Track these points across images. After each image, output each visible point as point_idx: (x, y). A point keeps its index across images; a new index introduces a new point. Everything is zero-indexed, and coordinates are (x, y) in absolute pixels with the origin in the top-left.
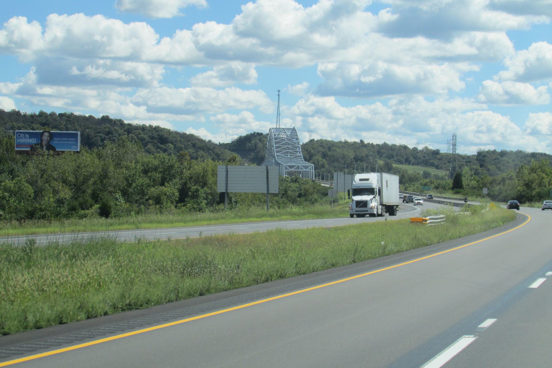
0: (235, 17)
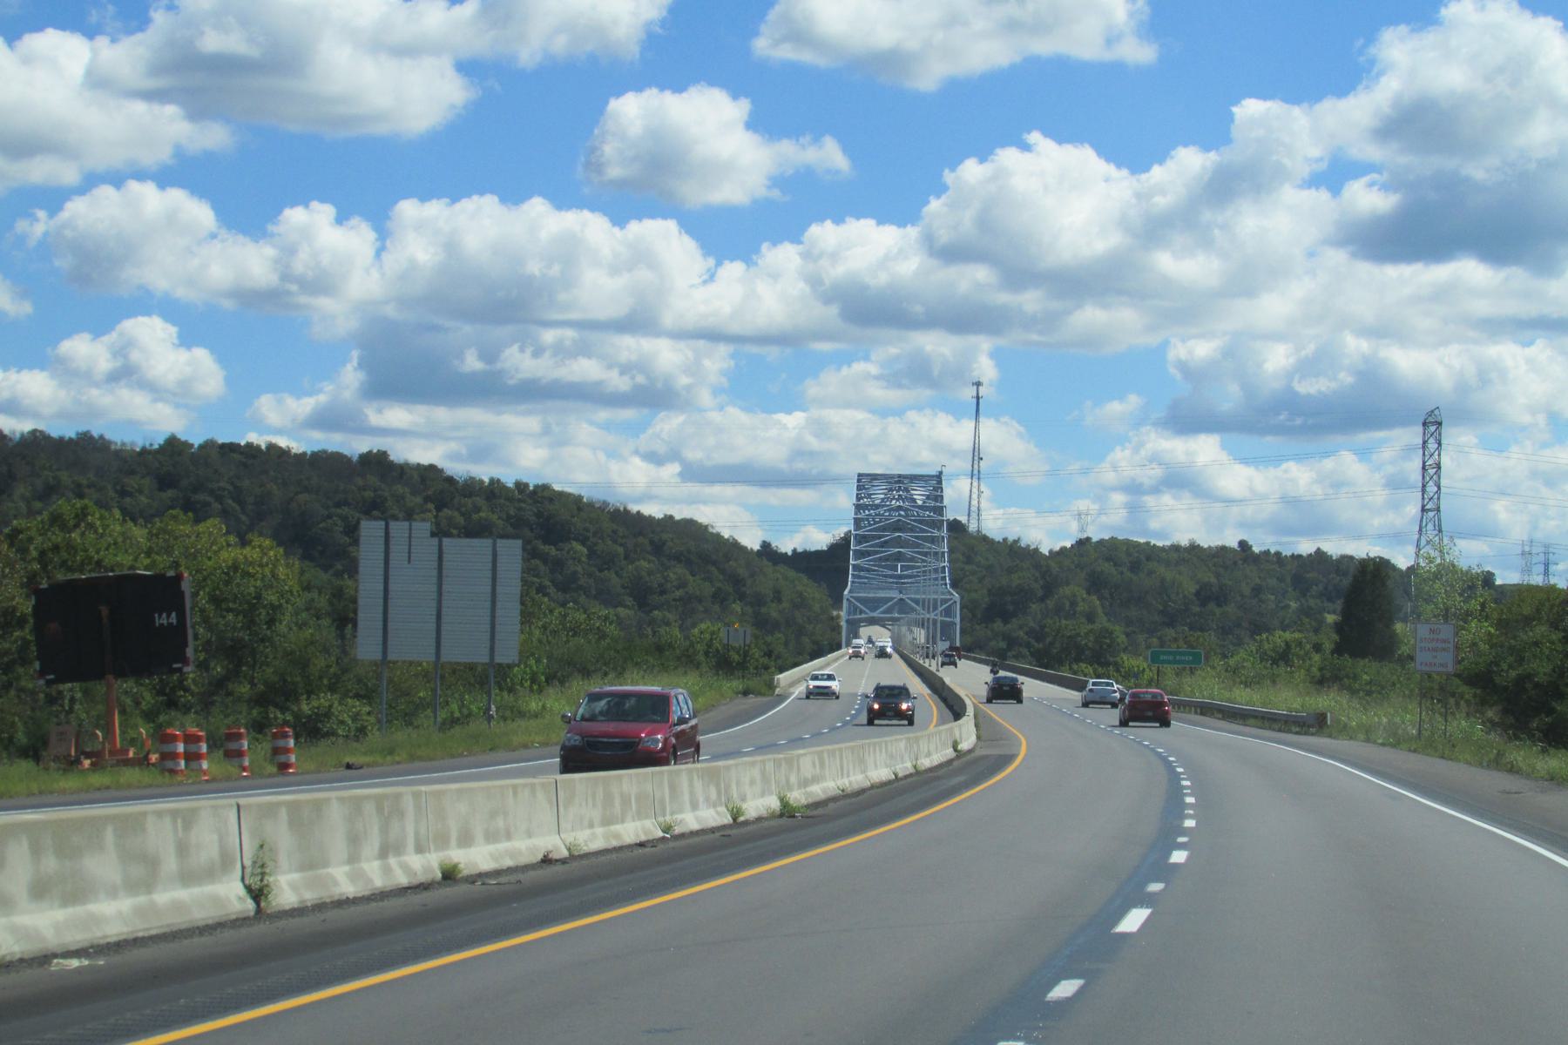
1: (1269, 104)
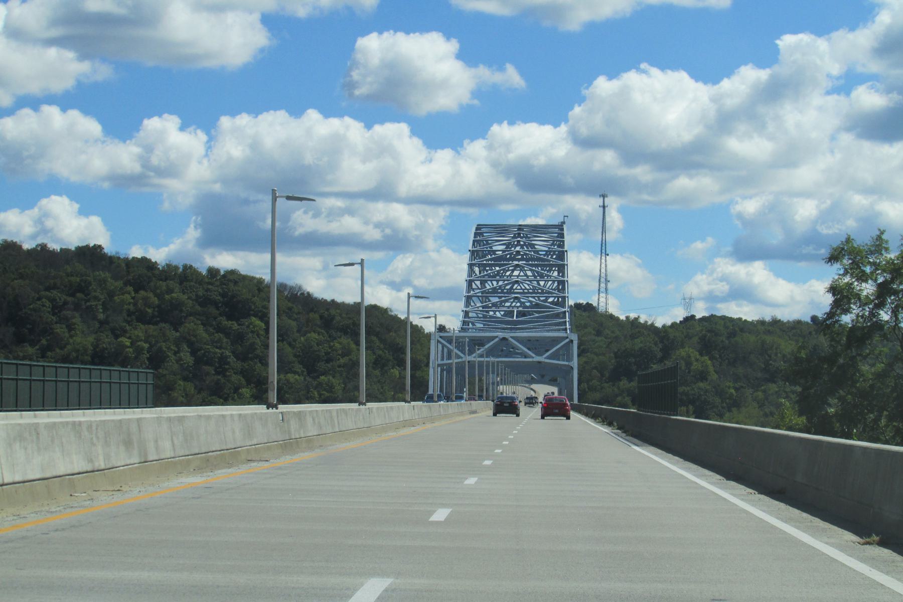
0: (572, 109)
1: (801, 36)
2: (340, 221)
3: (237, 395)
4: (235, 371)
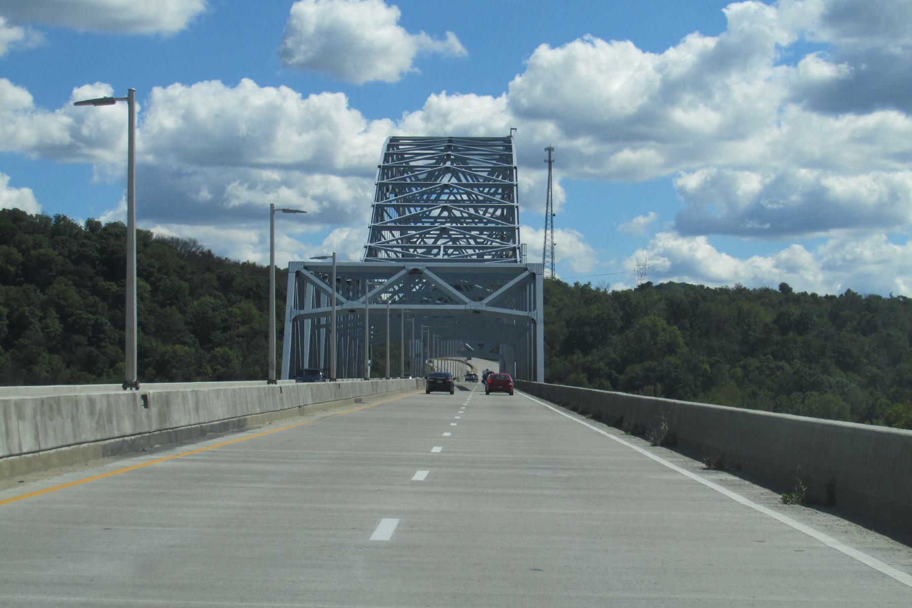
0: (513, 79)
2: (277, 192)
3: (113, 371)
4: (111, 341)
